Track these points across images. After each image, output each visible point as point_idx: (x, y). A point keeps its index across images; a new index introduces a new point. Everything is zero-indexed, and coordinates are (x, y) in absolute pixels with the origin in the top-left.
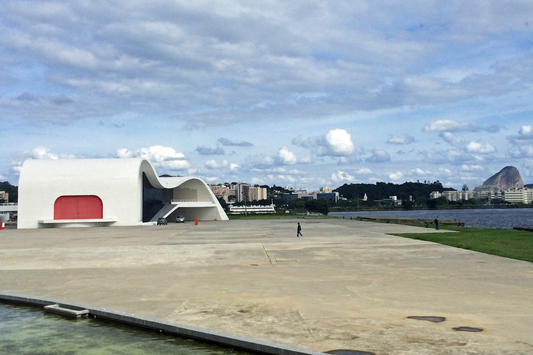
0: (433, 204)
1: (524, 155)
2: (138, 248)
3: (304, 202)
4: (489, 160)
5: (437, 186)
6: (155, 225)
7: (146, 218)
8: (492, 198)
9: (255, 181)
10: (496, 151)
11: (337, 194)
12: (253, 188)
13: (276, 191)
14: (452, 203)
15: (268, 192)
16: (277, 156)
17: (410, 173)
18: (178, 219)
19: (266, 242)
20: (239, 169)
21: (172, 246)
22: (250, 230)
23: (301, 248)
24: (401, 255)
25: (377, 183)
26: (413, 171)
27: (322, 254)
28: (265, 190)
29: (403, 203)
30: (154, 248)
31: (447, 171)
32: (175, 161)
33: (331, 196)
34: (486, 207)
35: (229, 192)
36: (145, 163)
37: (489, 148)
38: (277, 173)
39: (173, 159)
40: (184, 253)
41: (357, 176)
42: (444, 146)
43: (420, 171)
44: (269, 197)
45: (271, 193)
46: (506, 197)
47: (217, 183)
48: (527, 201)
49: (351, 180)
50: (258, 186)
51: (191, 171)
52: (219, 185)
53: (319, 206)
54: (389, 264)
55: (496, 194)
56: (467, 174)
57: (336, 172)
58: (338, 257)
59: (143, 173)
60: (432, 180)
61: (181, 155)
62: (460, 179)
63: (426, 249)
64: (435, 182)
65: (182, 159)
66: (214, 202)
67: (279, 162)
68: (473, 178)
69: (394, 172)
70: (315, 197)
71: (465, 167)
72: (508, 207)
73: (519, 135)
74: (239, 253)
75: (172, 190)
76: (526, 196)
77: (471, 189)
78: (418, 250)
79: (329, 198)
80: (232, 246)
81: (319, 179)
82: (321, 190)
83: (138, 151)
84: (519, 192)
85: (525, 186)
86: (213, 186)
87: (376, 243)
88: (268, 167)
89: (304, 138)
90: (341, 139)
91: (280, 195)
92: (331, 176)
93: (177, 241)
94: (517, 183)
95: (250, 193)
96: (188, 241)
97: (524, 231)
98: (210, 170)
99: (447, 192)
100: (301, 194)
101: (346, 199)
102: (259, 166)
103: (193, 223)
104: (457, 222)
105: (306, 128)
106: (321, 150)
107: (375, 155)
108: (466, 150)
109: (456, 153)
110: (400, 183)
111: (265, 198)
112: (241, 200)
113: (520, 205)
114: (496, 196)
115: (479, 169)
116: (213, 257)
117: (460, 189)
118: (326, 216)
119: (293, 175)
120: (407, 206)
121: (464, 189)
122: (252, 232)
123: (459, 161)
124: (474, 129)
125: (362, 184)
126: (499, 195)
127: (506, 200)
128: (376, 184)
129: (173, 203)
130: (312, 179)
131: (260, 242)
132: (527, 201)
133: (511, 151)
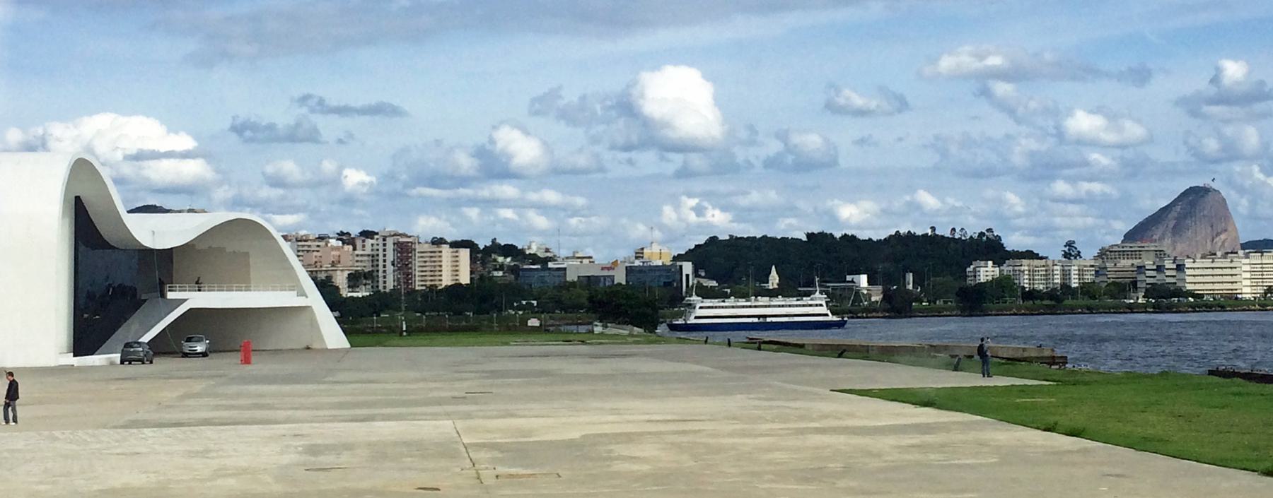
0: (975, 301)
1: (1231, 153)
2: (56, 439)
3: (586, 293)
4: (1134, 167)
5: (990, 247)
6: (112, 363)
7: (86, 338)
8: (1150, 281)
9: (424, 227)
10: (1150, 140)
11: (688, 268)
12: (427, 247)
13: (500, 259)
14: (1031, 295)
15: (473, 260)
16: (488, 147)
17: (897, 205)
18: (187, 347)
19: (468, 416)
20: (375, 191)
21: (166, 431)
22: (417, 381)
23: (575, 435)
24: (879, 455)
25: (809, 236)
26: (908, 198)
27: (637, 454)
28: (465, 254)
29: (887, 296)
30: (108, 436)
31: (1012, 198)
32: (166, 164)
33: (669, 274)
34: (1132, 309)
35: (351, 260)
36: (82, 168)
37: (1134, 131)
38: (491, 204)
39: (156, 156)
40: (205, 453)
41: (742, 214)
42: (998, 125)
43: (928, 200)
44: (476, 276)
45: (484, 264)
46: (1189, 279)
47: (313, 234)
48: (1248, 290)
49: (722, 223)
50: (446, 243)
51: (221, 194)
52: (321, 238)
53: (635, 304)
54: (841, 484)
55: (1160, 269)
56: (1072, 208)
57: (675, 202)
58: (687, 462)
59: (78, 199)
60: (972, 227)
61: (185, 142)
62: (1059, 224)
63: (957, 437)
64: (982, 234)
65: (186, 155)
66: (302, 294)
67: (495, 167)
68: (1090, 221)
69: (852, 201)
70: (620, 278)
71: (1061, 187)
72: (1194, 308)
73: (1213, 90)
74: (381, 453)
75: (168, 254)
76: (1248, 275)
77: (1089, 254)
78: (929, 438)
79: (663, 280)
80: (358, 431)
81: (624, 221)
82: (639, 254)
83: (40, 131)
84: (1226, 263)
85: (1244, 246)
86: (299, 241)
87: (802, 418)
88: (464, 181)
89: (570, 96)
90: (682, 97)
91: (514, 270)
92: (659, 212)
93: (184, 416)
94: (1223, 237)
95: (417, 263)
96: (225, 414)
97: (1239, 380)
98: (280, 191)
99: (1018, 262)
100: (577, 268)
101: (714, 284)
102: (433, 180)
103: (237, 357)
104: (1047, 353)
105: (573, 63)
106: (620, 129)
107: (789, 149)
108: (1060, 135)
109: (1033, 145)
110: (879, 235)
111: (465, 279)
112: (390, 285)
113: (1231, 302)
114: (1160, 277)
115: (1104, 194)
116: (298, 465)
117: (1056, 254)
118: (653, 337)
119: (542, 208)
120: (896, 306)
121: (1067, 255)
122: (421, 385)
123: (1041, 171)
124: (1080, 69)
125: (765, 237)
126: (1168, 273)
127: (1189, 287)
128: (805, 239)
129: (170, 295)
130: (598, 222)
131: (448, 415)
132: (1248, 290)
133: (1192, 141)
